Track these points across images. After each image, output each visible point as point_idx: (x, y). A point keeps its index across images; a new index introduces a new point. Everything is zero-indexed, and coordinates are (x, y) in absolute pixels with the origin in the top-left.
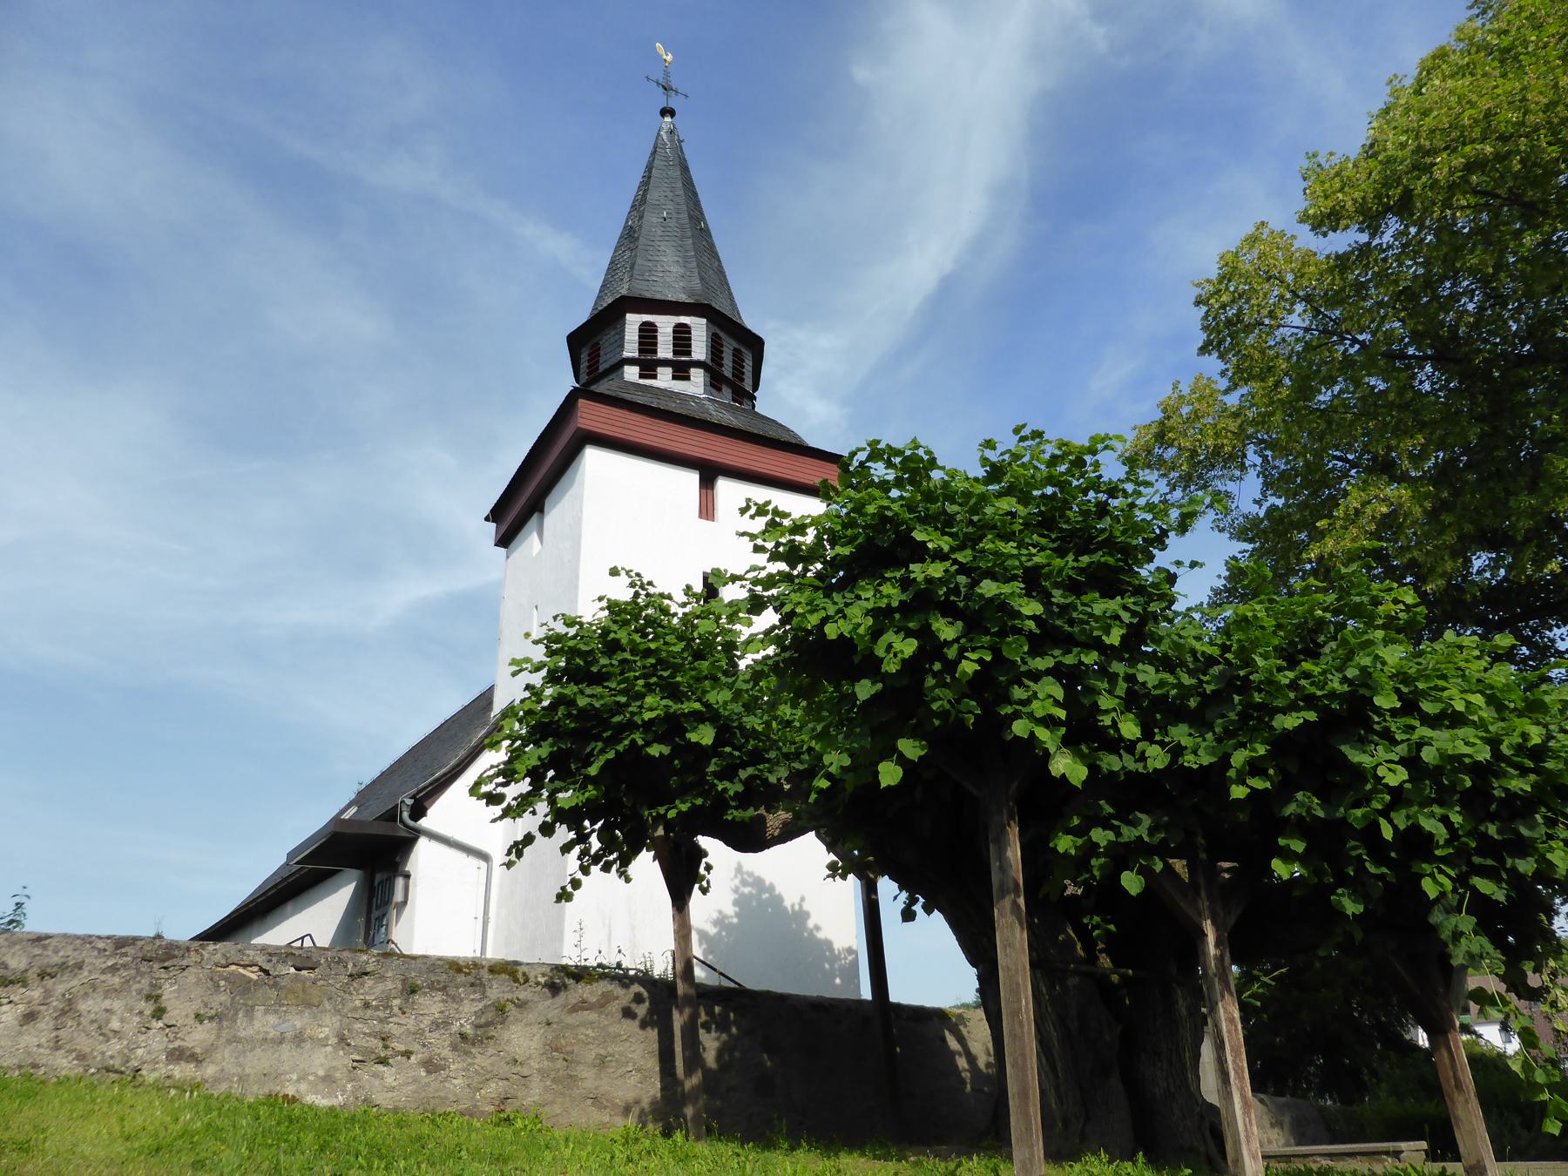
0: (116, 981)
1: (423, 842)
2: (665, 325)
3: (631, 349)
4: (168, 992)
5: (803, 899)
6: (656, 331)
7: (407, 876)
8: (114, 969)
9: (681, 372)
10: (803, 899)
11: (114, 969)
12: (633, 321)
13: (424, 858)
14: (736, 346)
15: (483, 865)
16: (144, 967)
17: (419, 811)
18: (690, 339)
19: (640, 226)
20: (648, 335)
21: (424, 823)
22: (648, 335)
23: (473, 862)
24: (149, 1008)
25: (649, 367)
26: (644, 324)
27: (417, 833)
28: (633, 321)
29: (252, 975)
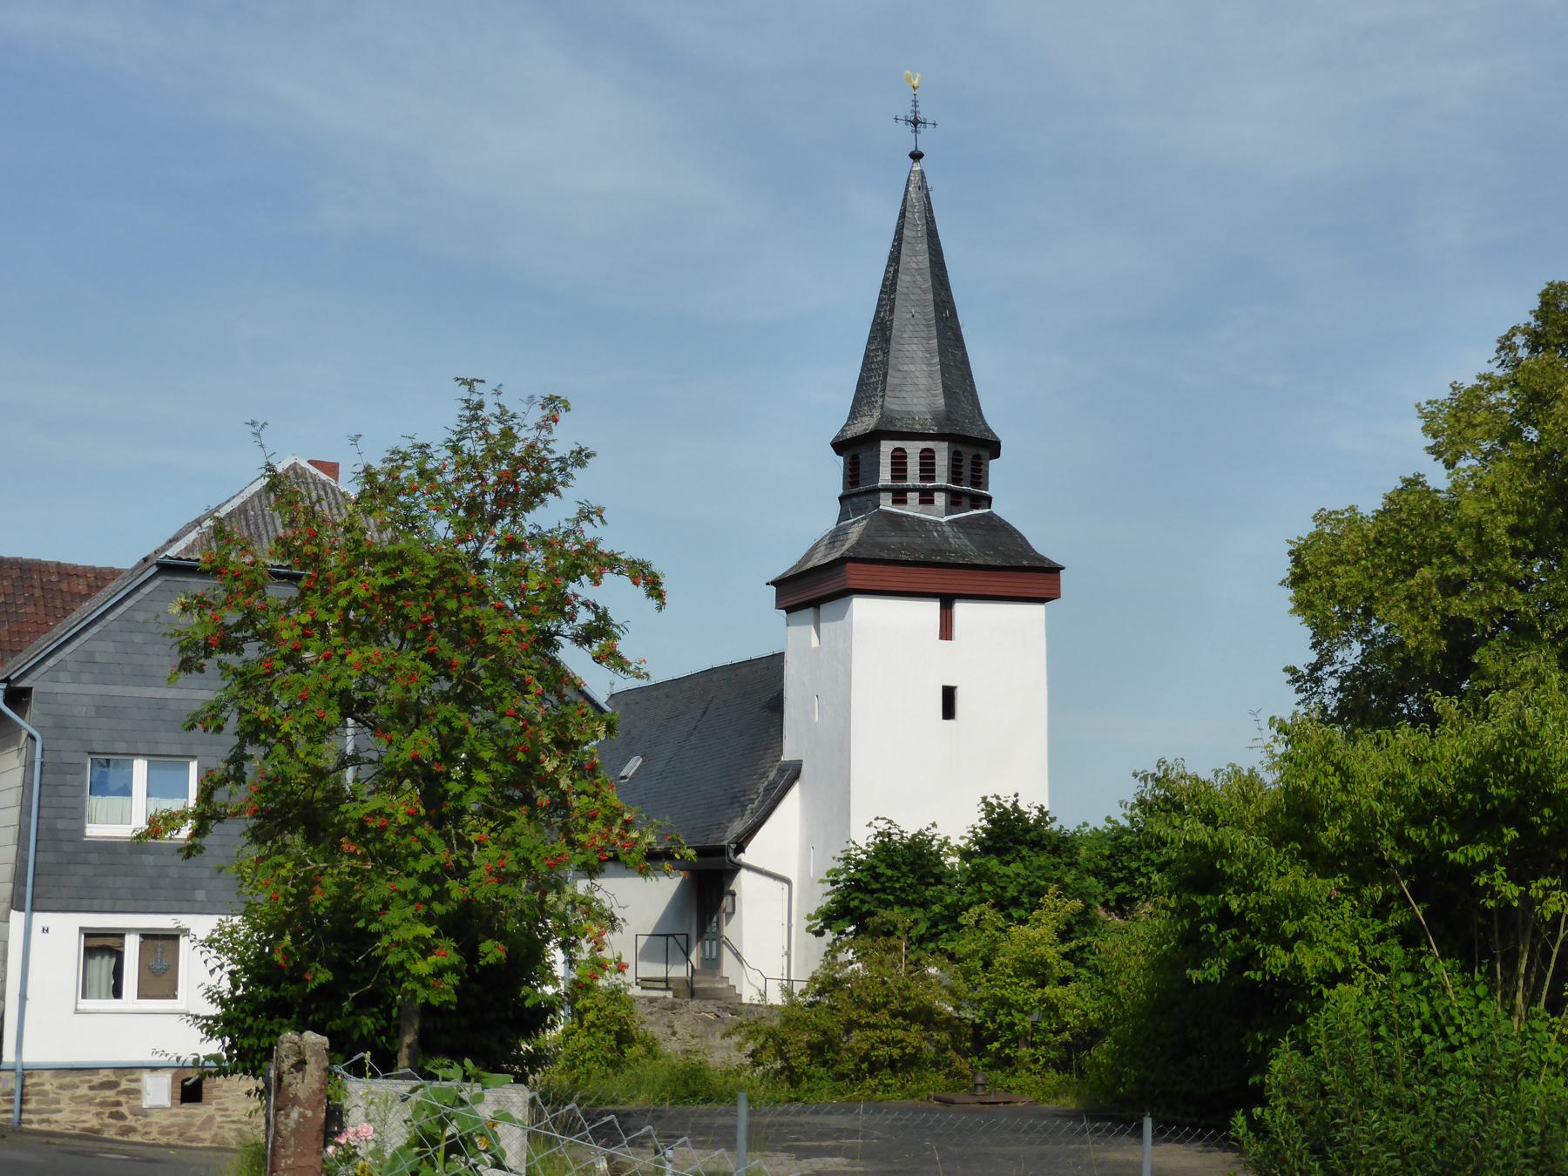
0: (653, 1018)
1: (743, 873)
2: (913, 449)
3: (885, 477)
4: (677, 1024)
5: (946, 631)
6: (906, 457)
7: (733, 894)
8: (651, 1013)
9: (926, 497)
10: (946, 631)
11: (651, 1013)
12: (887, 447)
13: (744, 883)
14: (974, 452)
15: (786, 886)
16: (664, 1012)
17: (740, 849)
18: (934, 464)
19: (891, 321)
20: (899, 459)
21: (743, 858)
22: (899, 459)
23: (778, 885)
24: (669, 1032)
25: (899, 496)
26: (896, 450)
27: (738, 867)
28: (887, 447)
29: (712, 1017)
